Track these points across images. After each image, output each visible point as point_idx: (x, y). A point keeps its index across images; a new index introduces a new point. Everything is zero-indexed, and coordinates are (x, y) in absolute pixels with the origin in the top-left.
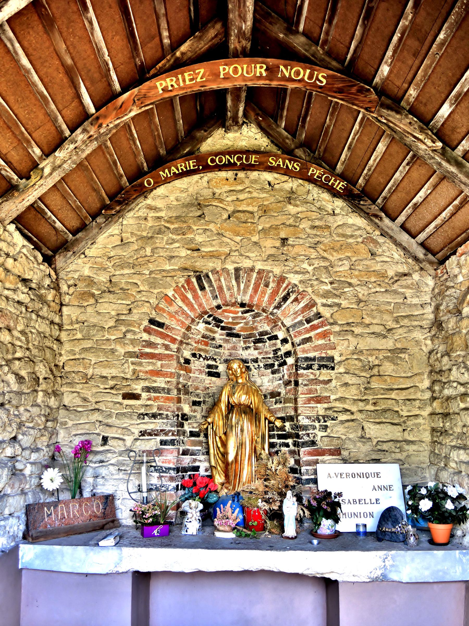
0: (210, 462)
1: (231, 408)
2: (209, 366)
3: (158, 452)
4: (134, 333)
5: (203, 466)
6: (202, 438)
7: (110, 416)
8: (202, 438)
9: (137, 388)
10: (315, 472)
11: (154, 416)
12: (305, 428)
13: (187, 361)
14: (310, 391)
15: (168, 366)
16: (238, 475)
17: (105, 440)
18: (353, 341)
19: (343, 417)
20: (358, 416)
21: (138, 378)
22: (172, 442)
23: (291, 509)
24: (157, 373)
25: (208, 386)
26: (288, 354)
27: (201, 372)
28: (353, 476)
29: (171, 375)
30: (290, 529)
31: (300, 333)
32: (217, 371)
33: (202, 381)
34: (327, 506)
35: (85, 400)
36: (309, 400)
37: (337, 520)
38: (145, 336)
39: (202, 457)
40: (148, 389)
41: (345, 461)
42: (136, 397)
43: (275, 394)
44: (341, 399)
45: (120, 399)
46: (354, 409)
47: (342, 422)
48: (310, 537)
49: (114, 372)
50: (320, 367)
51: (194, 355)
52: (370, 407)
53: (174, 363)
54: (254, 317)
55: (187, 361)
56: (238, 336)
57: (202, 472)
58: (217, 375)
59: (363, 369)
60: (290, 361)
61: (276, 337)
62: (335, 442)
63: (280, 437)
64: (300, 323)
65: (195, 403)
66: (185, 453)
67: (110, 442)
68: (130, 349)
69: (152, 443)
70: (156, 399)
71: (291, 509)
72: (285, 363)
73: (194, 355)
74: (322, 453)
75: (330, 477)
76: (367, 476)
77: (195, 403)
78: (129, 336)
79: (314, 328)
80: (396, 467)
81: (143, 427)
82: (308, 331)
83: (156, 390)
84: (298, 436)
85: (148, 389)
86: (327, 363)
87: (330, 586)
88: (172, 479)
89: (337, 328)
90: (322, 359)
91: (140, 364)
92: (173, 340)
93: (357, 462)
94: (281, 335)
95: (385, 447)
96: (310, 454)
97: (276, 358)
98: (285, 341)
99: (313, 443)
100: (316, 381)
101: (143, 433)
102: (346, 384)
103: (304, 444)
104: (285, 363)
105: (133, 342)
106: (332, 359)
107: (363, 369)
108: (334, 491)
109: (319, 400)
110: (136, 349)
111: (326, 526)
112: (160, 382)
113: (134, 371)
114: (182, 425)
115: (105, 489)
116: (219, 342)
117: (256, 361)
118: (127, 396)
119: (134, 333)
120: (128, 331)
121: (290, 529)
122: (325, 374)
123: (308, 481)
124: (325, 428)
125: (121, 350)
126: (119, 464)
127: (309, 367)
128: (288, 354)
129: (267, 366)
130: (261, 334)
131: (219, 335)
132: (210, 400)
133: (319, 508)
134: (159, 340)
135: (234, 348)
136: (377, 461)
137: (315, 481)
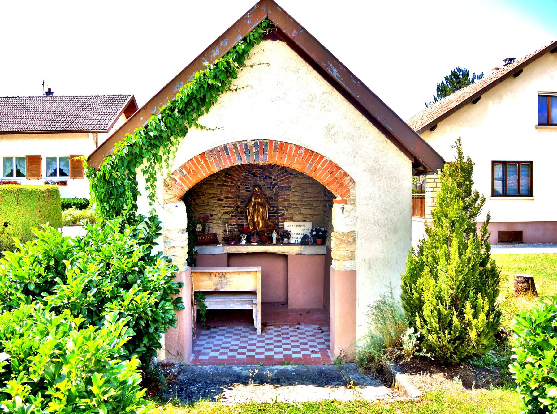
0: (247, 222)
1: (255, 203)
2: (247, 188)
3: (231, 219)
4: (220, 177)
5: (245, 224)
6: (244, 214)
7: (213, 207)
8: (244, 214)
9: (222, 197)
10: (284, 225)
11: (229, 207)
12: (281, 210)
13: (239, 187)
14: (283, 198)
15: (233, 189)
16: (258, 226)
17: (212, 215)
18: (298, 180)
19: (294, 207)
20: (299, 206)
21: (222, 194)
22: (235, 216)
23: (275, 235)
24: (229, 192)
25: (454, 271)
26: (276, 184)
27: (244, 190)
28: (296, 226)
29: (234, 192)
30: (274, 241)
31: (279, 178)
32: (473, 387)
33: (244, 193)
34: (287, 235)
35: (204, 201)
36: (282, 201)
37: (289, 239)
38: (224, 179)
39: (244, 221)
40: (226, 198)
41: (294, 221)
42: (222, 200)
43: (271, 198)
44: (294, 201)
45: (216, 201)
46: (298, 204)
47: (293, 208)
48: (280, 242)
49: (214, 192)
50: (286, 190)
51: (241, 184)
52: (303, 203)
53: (235, 188)
54: (264, 170)
55: (239, 187)
56: (257, 176)
57: (245, 225)
58: (249, 191)
59: (301, 190)
60: (276, 186)
61: (271, 178)
62: (291, 215)
63: (273, 213)
64: (280, 174)
65: (242, 202)
66: (239, 219)
67: (214, 216)
68: (219, 183)
69: (228, 216)
70: (229, 201)
71: (275, 235)
72: (274, 187)
73: (241, 184)
74: (286, 218)
75: (288, 226)
76: (301, 226)
77: (242, 202)
78: (218, 179)
79: (284, 176)
80: (311, 223)
81: (225, 211)
82: (282, 177)
83: (229, 198)
84: (278, 213)
85: (226, 198)
86: (289, 188)
87: (285, 257)
88: (235, 228)
89: (292, 176)
90: (287, 187)
91: (223, 189)
92: (235, 180)
93: (298, 221)
94: (273, 177)
95: (307, 216)
96: (282, 219)
97: (271, 185)
98: (274, 179)
99: (283, 215)
100: (285, 194)
101: (225, 213)
102: (295, 196)
103: (280, 216)
104: (274, 187)
105: (220, 181)
106: (290, 187)
107: (301, 190)
108: (289, 230)
109: (285, 201)
110: (221, 183)
111: (286, 240)
112: (230, 195)
113: (221, 191)
114: (237, 210)
115: (214, 231)
116: (250, 179)
117: (264, 185)
118: (219, 200)
119: (220, 177)
120: (218, 177)
121: (274, 241)
122: (288, 192)
123: (281, 228)
124: (287, 210)
125: (216, 184)
126: (216, 223)
127: (283, 190)
128: (276, 184)
129: (268, 188)
130: (266, 176)
131: (250, 176)
132: (247, 200)
133: (283, 235)
134: (229, 180)
135: (256, 181)
136: (305, 221)
137: (284, 228)
